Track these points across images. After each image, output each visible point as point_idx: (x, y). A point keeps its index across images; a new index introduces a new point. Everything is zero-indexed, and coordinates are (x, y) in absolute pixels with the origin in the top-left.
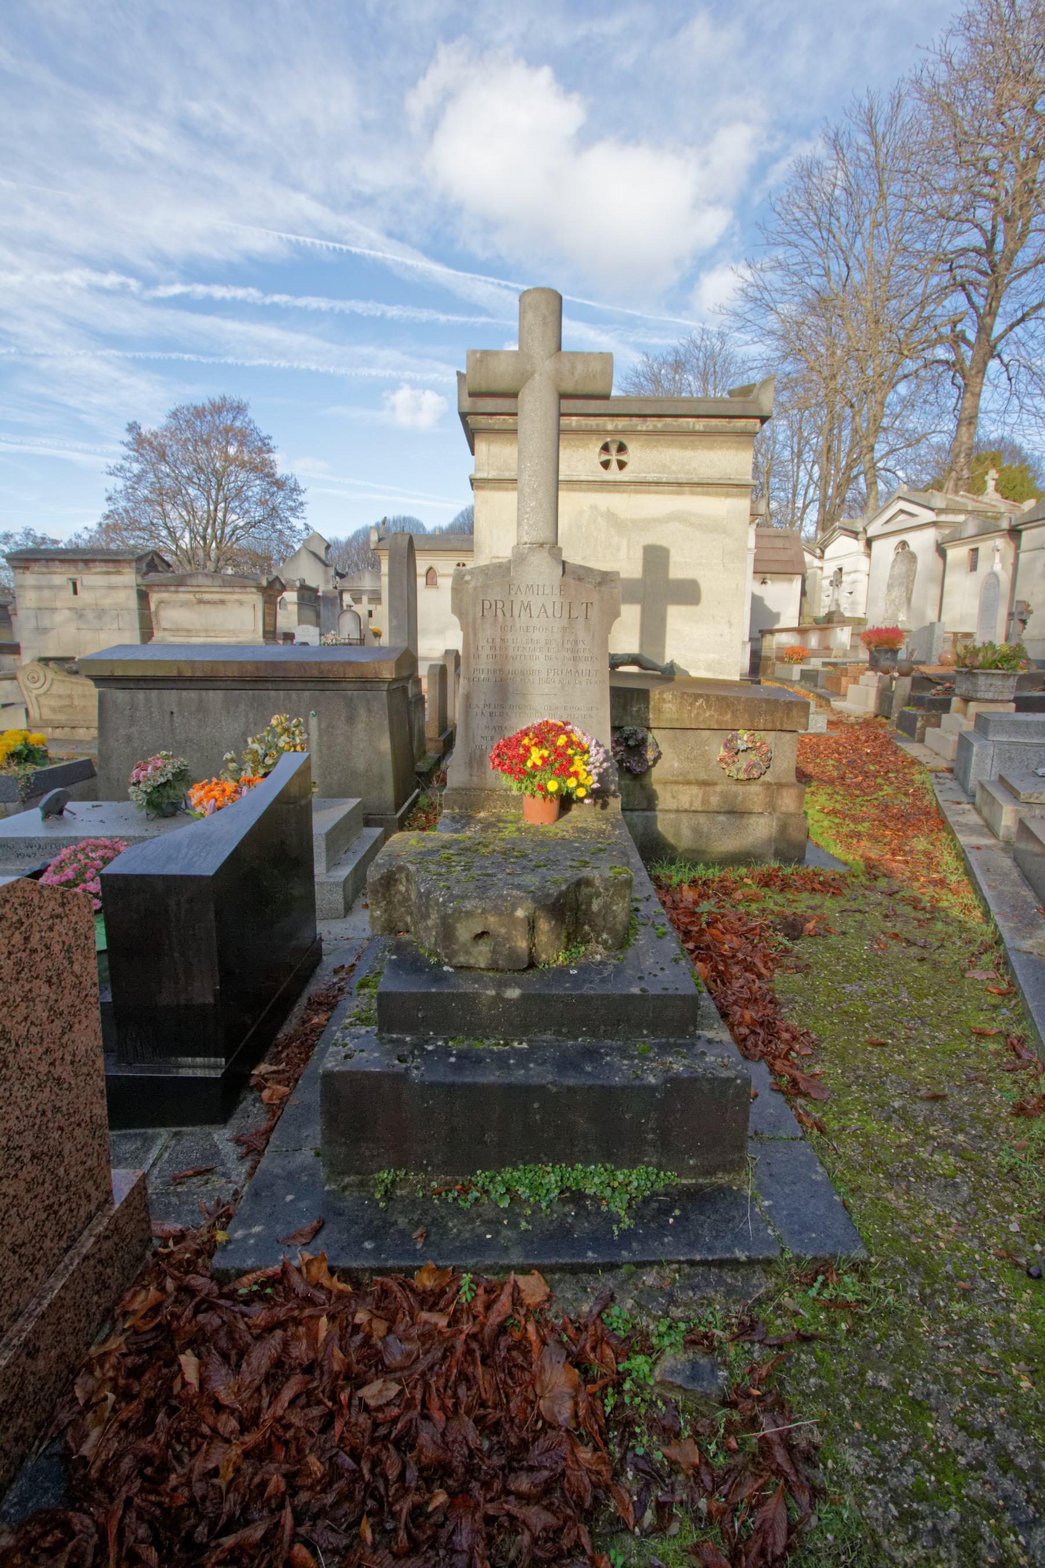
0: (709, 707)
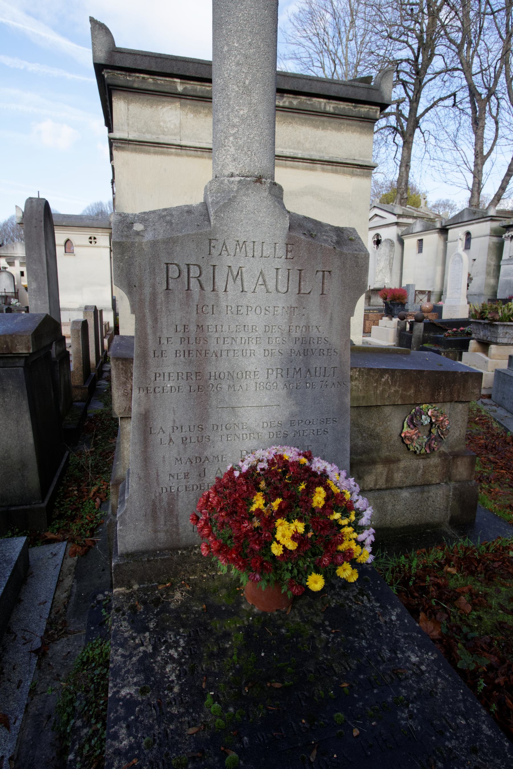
0: (394, 383)
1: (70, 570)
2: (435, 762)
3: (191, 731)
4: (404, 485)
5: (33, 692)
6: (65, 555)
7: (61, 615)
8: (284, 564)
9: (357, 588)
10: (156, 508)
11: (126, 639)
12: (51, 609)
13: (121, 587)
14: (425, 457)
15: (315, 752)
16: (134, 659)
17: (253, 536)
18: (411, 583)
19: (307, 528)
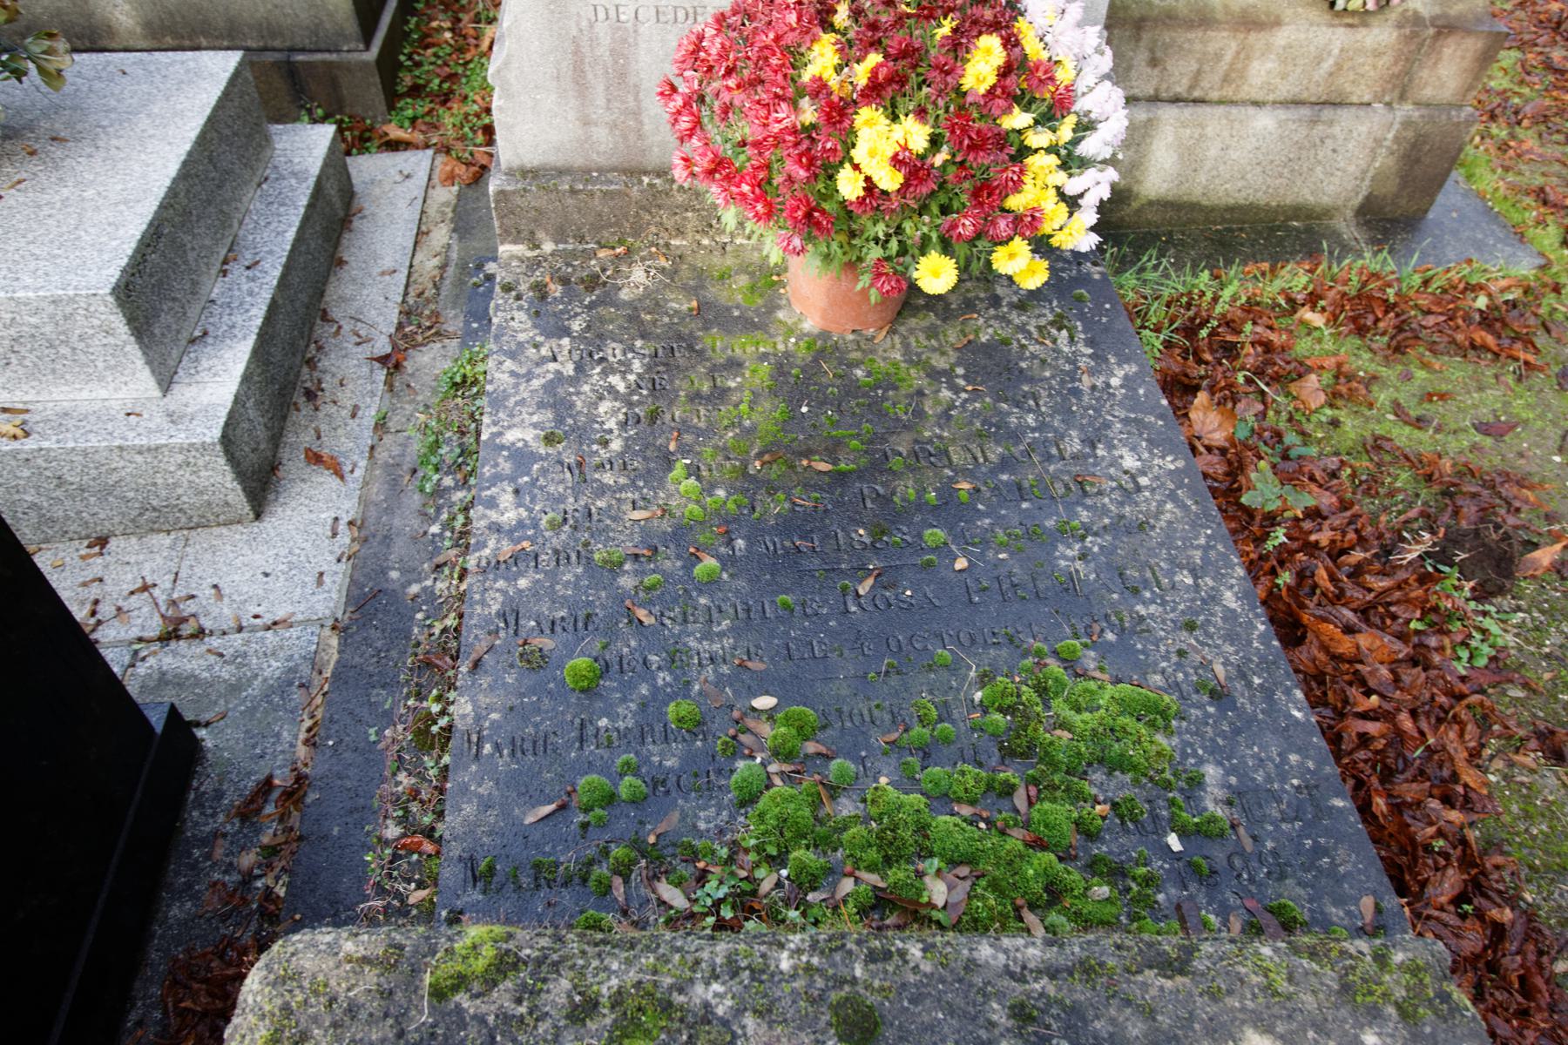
1: (443, 213)
2: (1102, 631)
3: (637, 515)
4: (1271, 98)
5: (381, 426)
6: (430, 179)
7: (428, 301)
8: (869, 224)
9: (1052, 310)
10: (582, 62)
11: (520, 345)
12: (407, 286)
13: (515, 242)
14: (1356, 21)
15: (870, 582)
16: (536, 383)
17: (796, 145)
18: (1204, 333)
19: (935, 142)
